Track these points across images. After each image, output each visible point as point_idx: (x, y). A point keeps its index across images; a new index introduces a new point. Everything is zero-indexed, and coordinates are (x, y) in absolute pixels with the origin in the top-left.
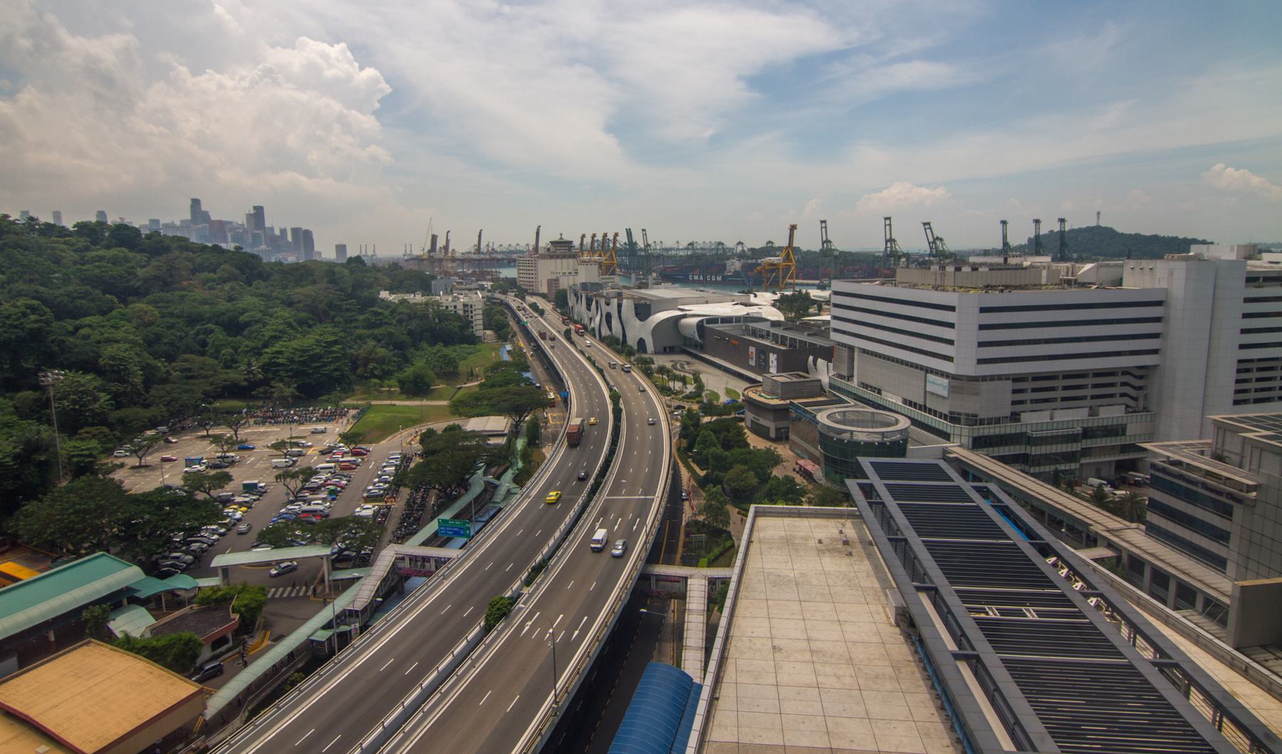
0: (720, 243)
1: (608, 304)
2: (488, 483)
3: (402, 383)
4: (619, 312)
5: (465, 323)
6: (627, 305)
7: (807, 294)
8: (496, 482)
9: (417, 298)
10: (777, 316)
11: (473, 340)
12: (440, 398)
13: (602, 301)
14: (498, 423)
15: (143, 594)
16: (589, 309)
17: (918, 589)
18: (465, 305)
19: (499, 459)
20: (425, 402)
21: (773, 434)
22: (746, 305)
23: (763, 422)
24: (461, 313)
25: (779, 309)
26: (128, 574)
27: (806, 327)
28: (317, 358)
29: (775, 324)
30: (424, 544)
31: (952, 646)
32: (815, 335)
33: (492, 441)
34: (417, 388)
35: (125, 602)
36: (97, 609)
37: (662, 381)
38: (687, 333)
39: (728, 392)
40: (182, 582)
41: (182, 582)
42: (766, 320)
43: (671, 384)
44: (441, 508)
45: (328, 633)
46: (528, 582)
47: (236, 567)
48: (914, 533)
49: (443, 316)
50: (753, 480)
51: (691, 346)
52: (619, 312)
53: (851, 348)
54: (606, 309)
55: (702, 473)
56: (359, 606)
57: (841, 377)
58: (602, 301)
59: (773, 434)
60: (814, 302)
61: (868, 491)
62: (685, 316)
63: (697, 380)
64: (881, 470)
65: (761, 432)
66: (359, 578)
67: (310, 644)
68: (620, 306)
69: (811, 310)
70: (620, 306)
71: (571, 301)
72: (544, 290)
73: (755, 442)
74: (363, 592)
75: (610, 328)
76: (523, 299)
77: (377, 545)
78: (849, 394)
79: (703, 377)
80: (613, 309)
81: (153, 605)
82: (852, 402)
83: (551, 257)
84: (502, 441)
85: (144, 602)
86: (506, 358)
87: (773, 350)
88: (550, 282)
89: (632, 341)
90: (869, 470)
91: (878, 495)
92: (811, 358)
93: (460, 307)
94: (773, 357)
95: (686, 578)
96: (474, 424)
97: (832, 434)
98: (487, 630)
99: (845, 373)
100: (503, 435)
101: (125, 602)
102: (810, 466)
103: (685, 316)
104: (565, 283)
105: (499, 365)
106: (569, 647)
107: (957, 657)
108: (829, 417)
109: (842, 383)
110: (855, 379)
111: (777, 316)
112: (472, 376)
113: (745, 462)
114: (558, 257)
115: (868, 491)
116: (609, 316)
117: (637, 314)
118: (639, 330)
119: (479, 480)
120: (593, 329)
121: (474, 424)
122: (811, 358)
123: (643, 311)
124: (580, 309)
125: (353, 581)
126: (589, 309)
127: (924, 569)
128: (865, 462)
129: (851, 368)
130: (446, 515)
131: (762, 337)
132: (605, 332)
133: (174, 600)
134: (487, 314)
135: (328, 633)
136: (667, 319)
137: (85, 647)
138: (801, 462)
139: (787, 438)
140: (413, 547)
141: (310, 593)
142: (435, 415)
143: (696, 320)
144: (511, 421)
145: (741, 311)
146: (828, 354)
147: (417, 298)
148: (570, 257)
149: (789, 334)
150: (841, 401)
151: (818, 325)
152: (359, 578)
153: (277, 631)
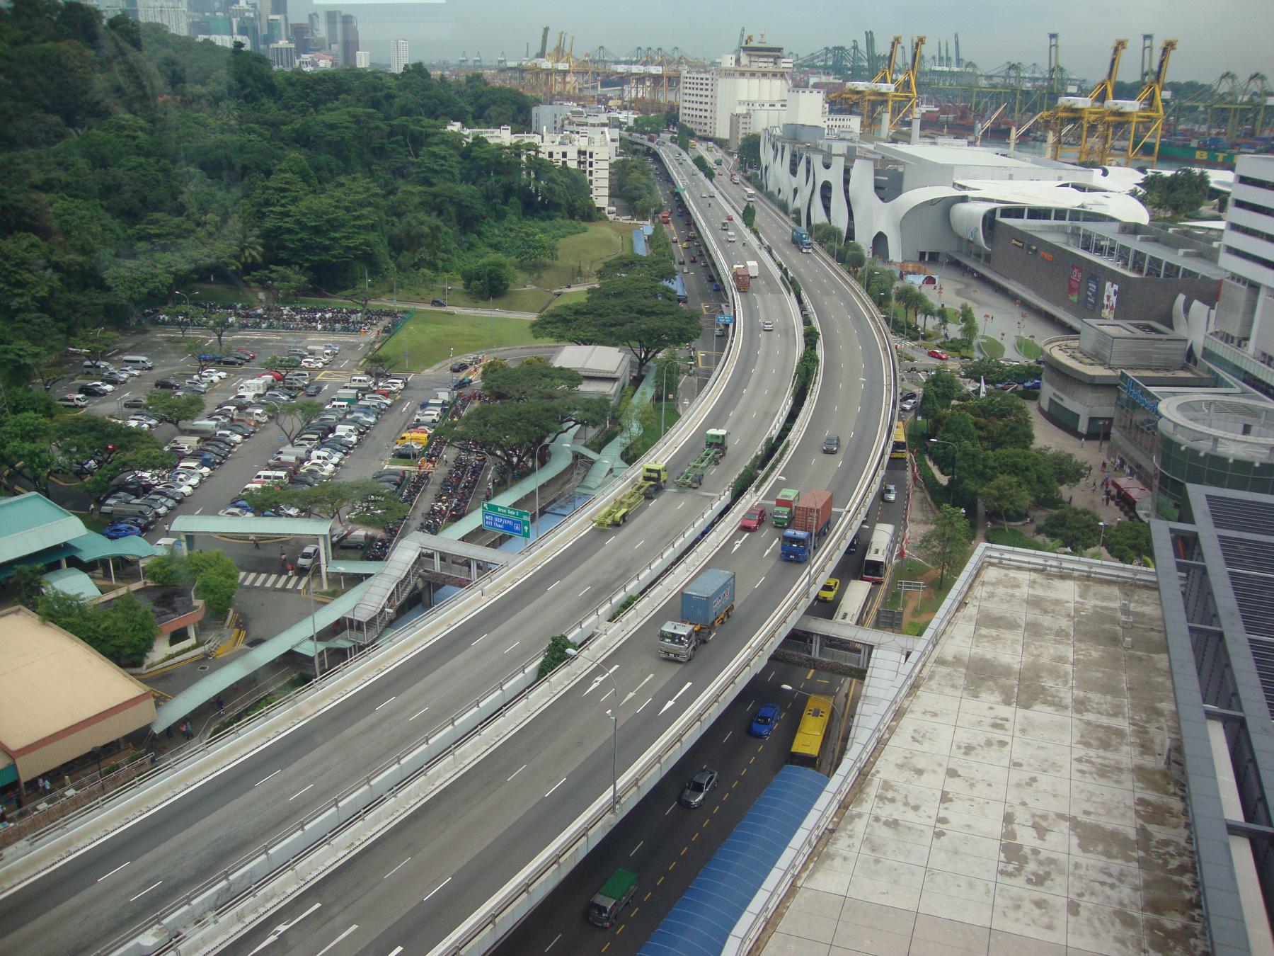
0: (1013, 67)
1: (827, 167)
2: (577, 456)
3: (468, 278)
4: (846, 181)
5: (577, 183)
6: (863, 177)
7: (1203, 179)
8: (592, 455)
9: (503, 136)
10: (1140, 215)
11: (591, 214)
12: (523, 308)
13: (817, 160)
14: (607, 359)
15: (87, 557)
16: (793, 172)
17: (1210, 715)
18: (581, 153)
19: (603, 421)
20: (498, 313)
21: (1083, 427)
22: (1081, 188)
23: (1070, 404)
24: (573, 165)
25: (1142, 200)
26: (67, 528)
27: (1186, 239)
28: (334, 225)
29: (1133, 229)
30: (465, 539)
31: (1234, 812)
32: (1200, 255)
33: (586, 387)
34: (490, 288)
35: (64, 564)
36: (26, 568)
37: (901, 311)
38: (962, 230)
39: (1022, 346)
40: (133, 546)
41: (133, 546)
42: (1112, 219)
43: (920, 320)
44: (502, 485)
45: (321, 647)
46: (613, 618)
47: (208, 536)
48: (1239, 625)
49: (541, 167)
50: (1025, 498)
51: (968, 254)
52: (846, 181)
53: (1254, 287)
54: (822, 175)
55: (944, 480)
56: (363, 616)
57: (1227, 338)
58: (817, 160)
59: (1083, 427)
60: (1215, 193)
61: (1186, 545)
62: (964, 199)
63: (966, 316)
64: (1222, 512)
65: (1062, 420)
66: (368, 576)
67: (291, 658)
68: (847, 171)
69: (1205, 209)
70: (847, 171)
71: (766, 155)
72: (723, 132)
73: (1046, 438)
74: (368, 600)
75: (827, 209)
76: (685, 147)
77: (394, 532)
78: (1237, 370)
79: (978, 315)
80: (834, 176)
81: (99, 572)
82: (1238, 386)
83: (742, 74)
84: (609, 389)
85: (88, 567)
86: (641, 249)
87: (1113, 276)
88: (735, 119)
89: (864, 240)
90: (1200, 508)
91: (1200, 554)
92: (1181, 298)
93: (572, 153)
94: (1110, 289)
95: (871, 647)
96: (571, 356)
97: (1179, 438)
98: (543, 672)
99: (1235, 332)
100: (614, 380)
101: (64, 564)
102: (1133, 487)
103: (964, 199)
104: (763, 122)
105: (629, 263)
106: (651, 724)
107: (1233, 829)
108: (1182, 408)
109: (1221, 349)
110: (1251, 347)
111: (1140, 215)
112: (577, 274)
113: (1014, 469)
114: (753, 74)
115: (1186, 545)
116: (826, 187)
117: (878, 188)
118: (876, 219)
119: (566, 443)
120: (798, 212)
121: (571, 356)
122: (1181, 298)
123: (888, 187)
124: (778, 173)
125: (356, 579)
126: (793, 172)
127: (1235, 684)
128: (1197, 494)
129: (1249, 324)
130: (504, 500)
131: (1099, 250)
132: (818, 216)
133: (124, 567)
134: (619, 172)
135: (321, 647)
136: (932, 203)
137: (13, 617)
138: (1123, 482)
139: (1107, 437)
140: (451, 539)
141: (301, 587)
142: (501, 333)
143: (984, 208)
144: (628, 357)
145: (1072, 200)
146: (1210, 293)
147: (503, 136)
148: (774, 75)
149: (1151, 250)
150: (1216, 382)
151: (1211, 236)
152: (368, 576)
153: (255, 634)
